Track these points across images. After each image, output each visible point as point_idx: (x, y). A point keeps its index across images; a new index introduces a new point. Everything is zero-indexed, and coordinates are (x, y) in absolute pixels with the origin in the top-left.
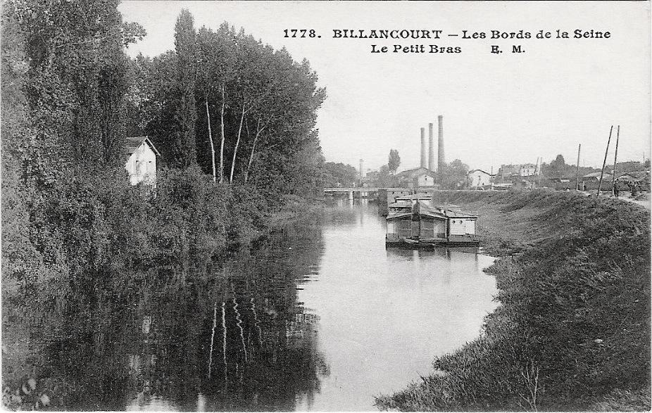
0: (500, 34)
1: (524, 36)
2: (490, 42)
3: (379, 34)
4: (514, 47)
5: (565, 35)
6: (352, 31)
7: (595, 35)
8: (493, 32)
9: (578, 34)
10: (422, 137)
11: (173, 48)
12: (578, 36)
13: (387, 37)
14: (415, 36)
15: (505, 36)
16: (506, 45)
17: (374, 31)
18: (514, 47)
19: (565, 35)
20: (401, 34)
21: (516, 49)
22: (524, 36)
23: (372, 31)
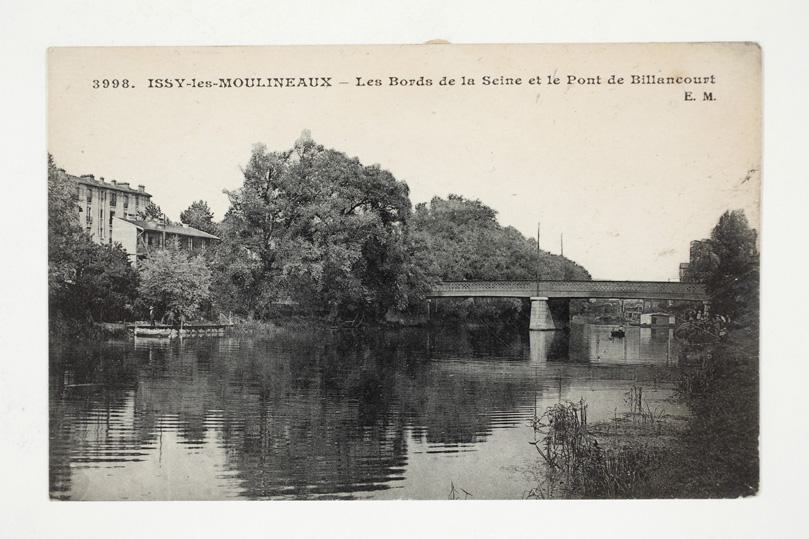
0: (399, 81)
1: (425, 82)
2: (679, 90)
3: (308, 82)
4: (705, 94)
5: (472, 82)
6: (259, 80)
7: (505, 82)
8: (391, 78)
9: (393, 81)
10: (449, 452)
11: (674, 276)
12: (487, 83)
13: (281, 85)
14: (651, 81)
15: (404, 83)
16: (698, 91)
17: (303, 79)
18: (705, 94)
19: (472, 82)
20: (234, 83)
21: (709, 97)
22: (425, 82)
23: (302, 79)
